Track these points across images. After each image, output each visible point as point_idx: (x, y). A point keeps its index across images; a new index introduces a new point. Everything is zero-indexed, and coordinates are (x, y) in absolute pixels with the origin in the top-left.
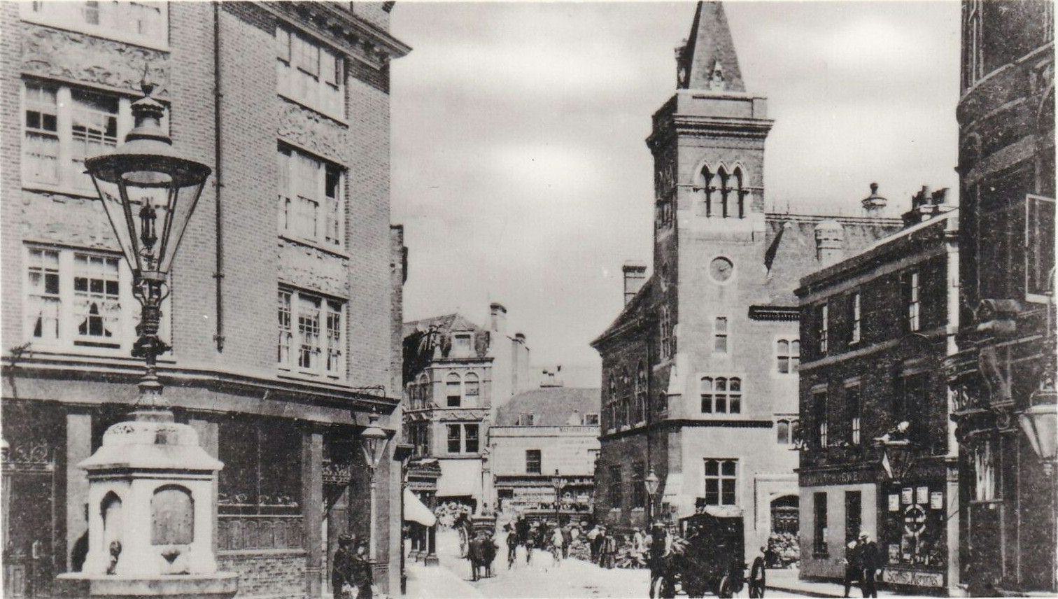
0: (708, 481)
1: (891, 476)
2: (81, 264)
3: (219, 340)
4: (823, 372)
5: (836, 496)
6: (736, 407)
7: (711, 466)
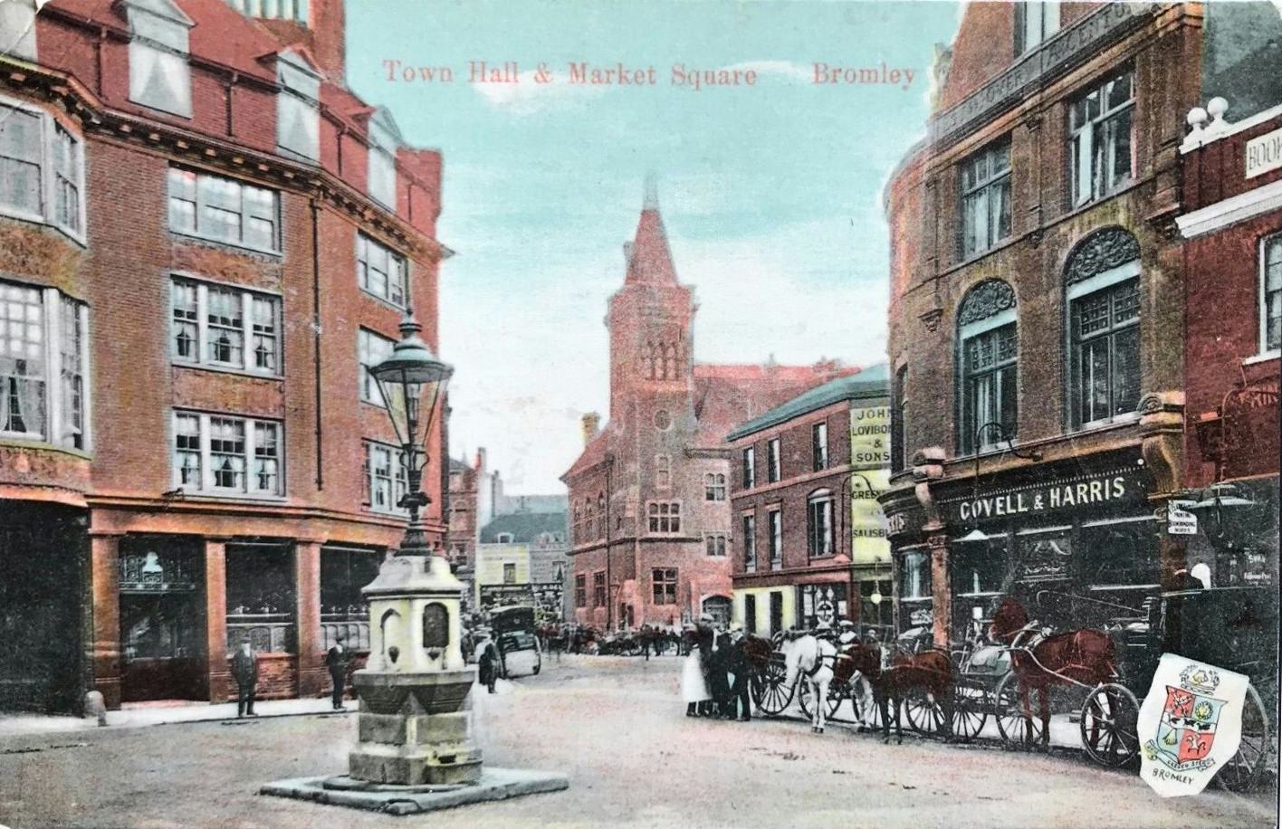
0: (655, 586)
1: (357, 672)
2: (216, 428)
3: (319, 482)
4: (751, 501)
5: (763, 597)
6: (676, 528)
7: (658, 574)
